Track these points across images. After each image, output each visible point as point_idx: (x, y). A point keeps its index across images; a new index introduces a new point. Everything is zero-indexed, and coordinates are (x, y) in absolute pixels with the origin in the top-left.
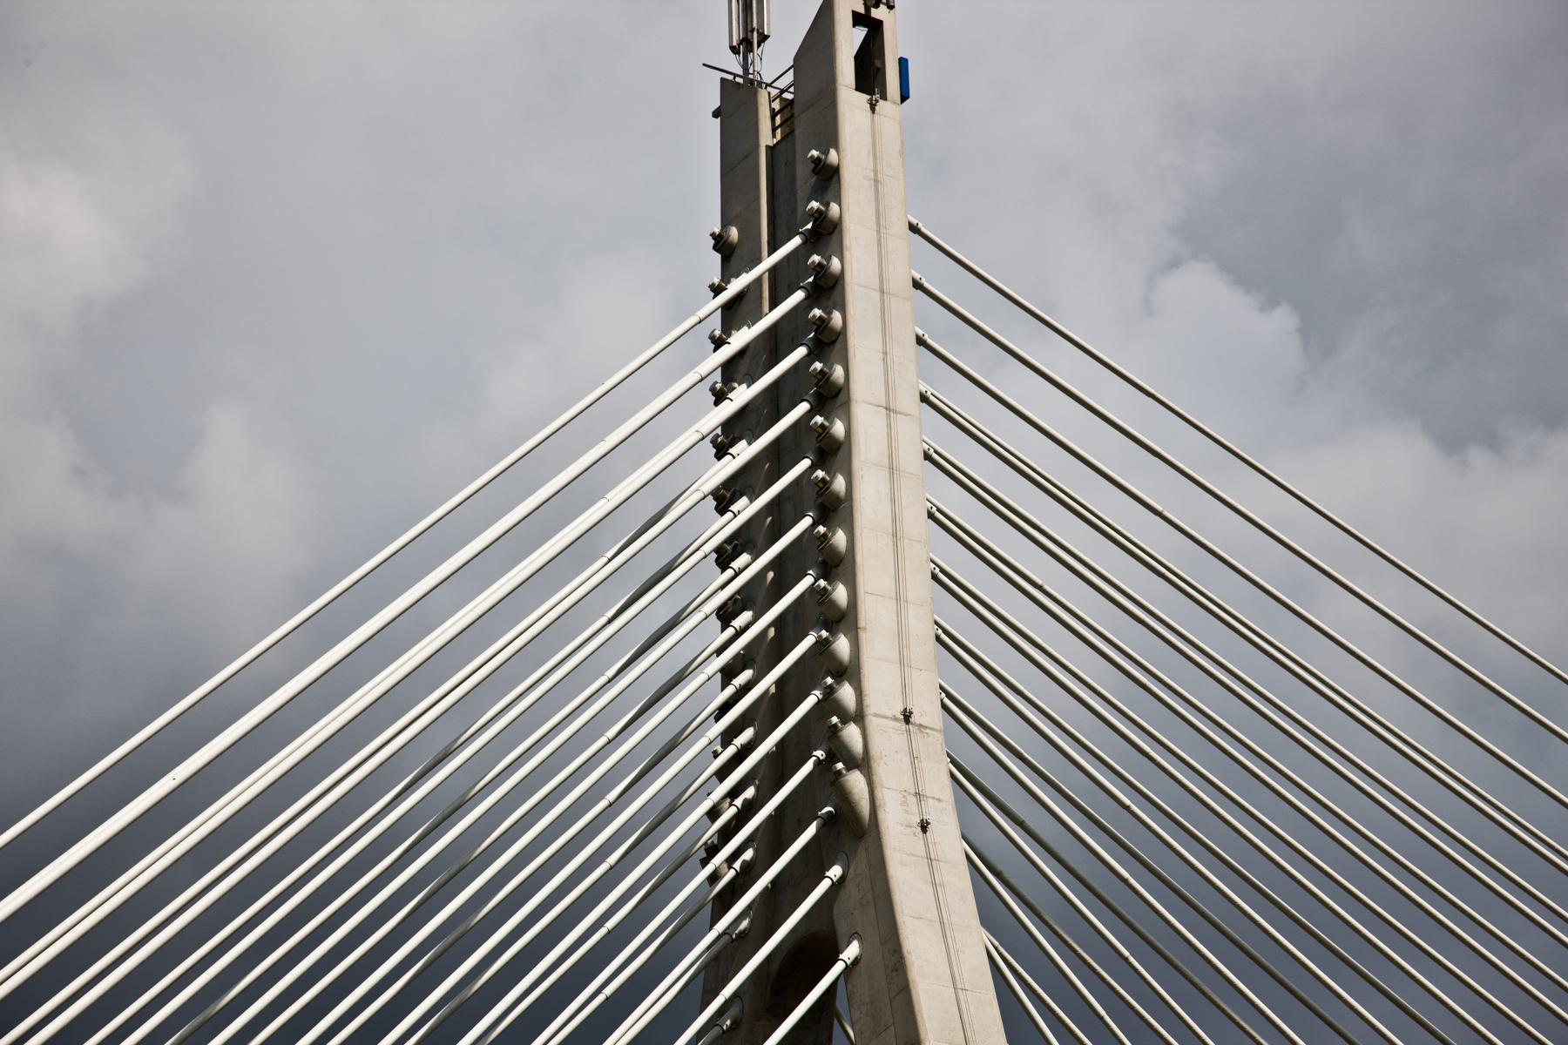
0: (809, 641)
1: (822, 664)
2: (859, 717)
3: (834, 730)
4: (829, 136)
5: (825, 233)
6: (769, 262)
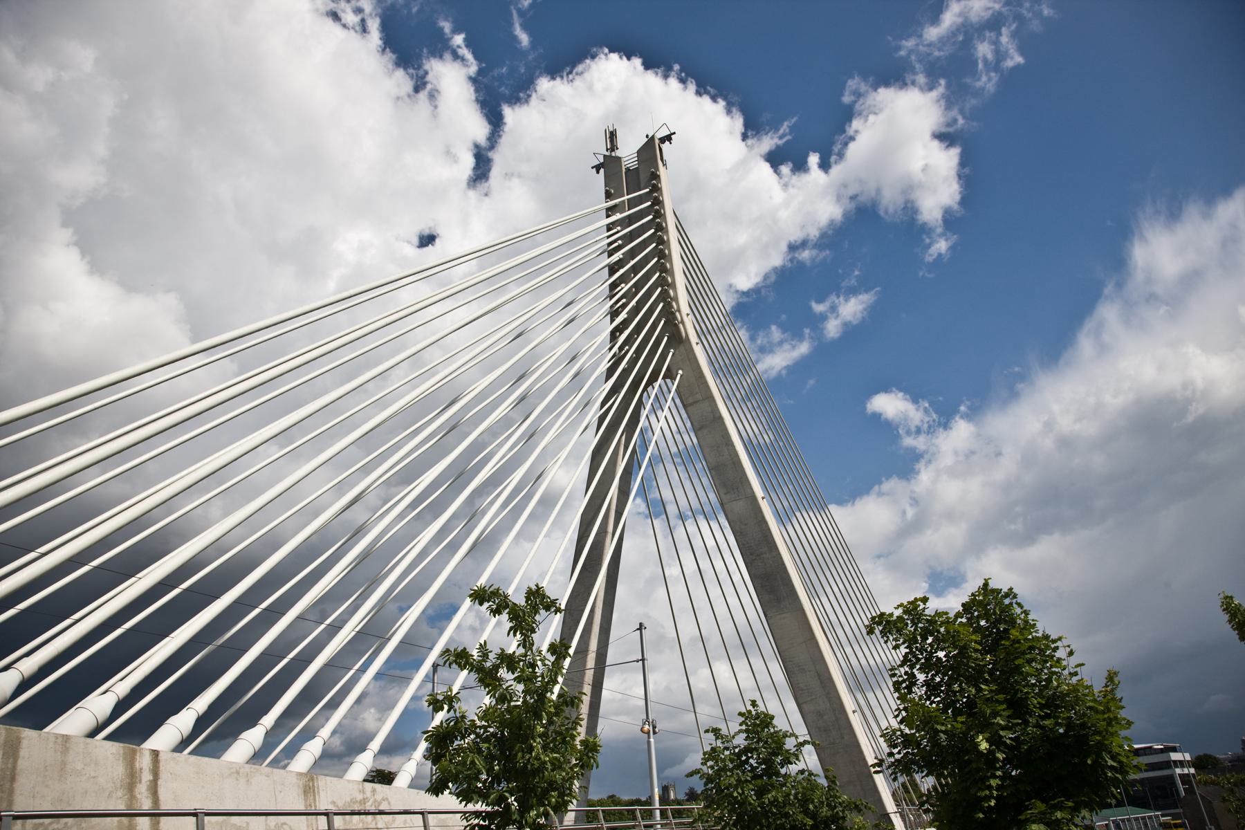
0: (659, 289)
1: (662, 282)
2: (679, 310)
3: (673, 314)
4: (657, 169)
5: (656, 189)
6: (626, 197)
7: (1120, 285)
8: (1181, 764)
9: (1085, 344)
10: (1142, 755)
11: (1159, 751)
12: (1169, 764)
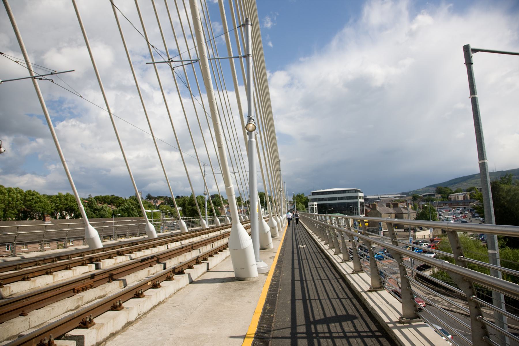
7: (355, 21)
8: (360, 197)
9: (334, 43)
10: (347, 193)
11: (354, 191)
12: (356, 197)
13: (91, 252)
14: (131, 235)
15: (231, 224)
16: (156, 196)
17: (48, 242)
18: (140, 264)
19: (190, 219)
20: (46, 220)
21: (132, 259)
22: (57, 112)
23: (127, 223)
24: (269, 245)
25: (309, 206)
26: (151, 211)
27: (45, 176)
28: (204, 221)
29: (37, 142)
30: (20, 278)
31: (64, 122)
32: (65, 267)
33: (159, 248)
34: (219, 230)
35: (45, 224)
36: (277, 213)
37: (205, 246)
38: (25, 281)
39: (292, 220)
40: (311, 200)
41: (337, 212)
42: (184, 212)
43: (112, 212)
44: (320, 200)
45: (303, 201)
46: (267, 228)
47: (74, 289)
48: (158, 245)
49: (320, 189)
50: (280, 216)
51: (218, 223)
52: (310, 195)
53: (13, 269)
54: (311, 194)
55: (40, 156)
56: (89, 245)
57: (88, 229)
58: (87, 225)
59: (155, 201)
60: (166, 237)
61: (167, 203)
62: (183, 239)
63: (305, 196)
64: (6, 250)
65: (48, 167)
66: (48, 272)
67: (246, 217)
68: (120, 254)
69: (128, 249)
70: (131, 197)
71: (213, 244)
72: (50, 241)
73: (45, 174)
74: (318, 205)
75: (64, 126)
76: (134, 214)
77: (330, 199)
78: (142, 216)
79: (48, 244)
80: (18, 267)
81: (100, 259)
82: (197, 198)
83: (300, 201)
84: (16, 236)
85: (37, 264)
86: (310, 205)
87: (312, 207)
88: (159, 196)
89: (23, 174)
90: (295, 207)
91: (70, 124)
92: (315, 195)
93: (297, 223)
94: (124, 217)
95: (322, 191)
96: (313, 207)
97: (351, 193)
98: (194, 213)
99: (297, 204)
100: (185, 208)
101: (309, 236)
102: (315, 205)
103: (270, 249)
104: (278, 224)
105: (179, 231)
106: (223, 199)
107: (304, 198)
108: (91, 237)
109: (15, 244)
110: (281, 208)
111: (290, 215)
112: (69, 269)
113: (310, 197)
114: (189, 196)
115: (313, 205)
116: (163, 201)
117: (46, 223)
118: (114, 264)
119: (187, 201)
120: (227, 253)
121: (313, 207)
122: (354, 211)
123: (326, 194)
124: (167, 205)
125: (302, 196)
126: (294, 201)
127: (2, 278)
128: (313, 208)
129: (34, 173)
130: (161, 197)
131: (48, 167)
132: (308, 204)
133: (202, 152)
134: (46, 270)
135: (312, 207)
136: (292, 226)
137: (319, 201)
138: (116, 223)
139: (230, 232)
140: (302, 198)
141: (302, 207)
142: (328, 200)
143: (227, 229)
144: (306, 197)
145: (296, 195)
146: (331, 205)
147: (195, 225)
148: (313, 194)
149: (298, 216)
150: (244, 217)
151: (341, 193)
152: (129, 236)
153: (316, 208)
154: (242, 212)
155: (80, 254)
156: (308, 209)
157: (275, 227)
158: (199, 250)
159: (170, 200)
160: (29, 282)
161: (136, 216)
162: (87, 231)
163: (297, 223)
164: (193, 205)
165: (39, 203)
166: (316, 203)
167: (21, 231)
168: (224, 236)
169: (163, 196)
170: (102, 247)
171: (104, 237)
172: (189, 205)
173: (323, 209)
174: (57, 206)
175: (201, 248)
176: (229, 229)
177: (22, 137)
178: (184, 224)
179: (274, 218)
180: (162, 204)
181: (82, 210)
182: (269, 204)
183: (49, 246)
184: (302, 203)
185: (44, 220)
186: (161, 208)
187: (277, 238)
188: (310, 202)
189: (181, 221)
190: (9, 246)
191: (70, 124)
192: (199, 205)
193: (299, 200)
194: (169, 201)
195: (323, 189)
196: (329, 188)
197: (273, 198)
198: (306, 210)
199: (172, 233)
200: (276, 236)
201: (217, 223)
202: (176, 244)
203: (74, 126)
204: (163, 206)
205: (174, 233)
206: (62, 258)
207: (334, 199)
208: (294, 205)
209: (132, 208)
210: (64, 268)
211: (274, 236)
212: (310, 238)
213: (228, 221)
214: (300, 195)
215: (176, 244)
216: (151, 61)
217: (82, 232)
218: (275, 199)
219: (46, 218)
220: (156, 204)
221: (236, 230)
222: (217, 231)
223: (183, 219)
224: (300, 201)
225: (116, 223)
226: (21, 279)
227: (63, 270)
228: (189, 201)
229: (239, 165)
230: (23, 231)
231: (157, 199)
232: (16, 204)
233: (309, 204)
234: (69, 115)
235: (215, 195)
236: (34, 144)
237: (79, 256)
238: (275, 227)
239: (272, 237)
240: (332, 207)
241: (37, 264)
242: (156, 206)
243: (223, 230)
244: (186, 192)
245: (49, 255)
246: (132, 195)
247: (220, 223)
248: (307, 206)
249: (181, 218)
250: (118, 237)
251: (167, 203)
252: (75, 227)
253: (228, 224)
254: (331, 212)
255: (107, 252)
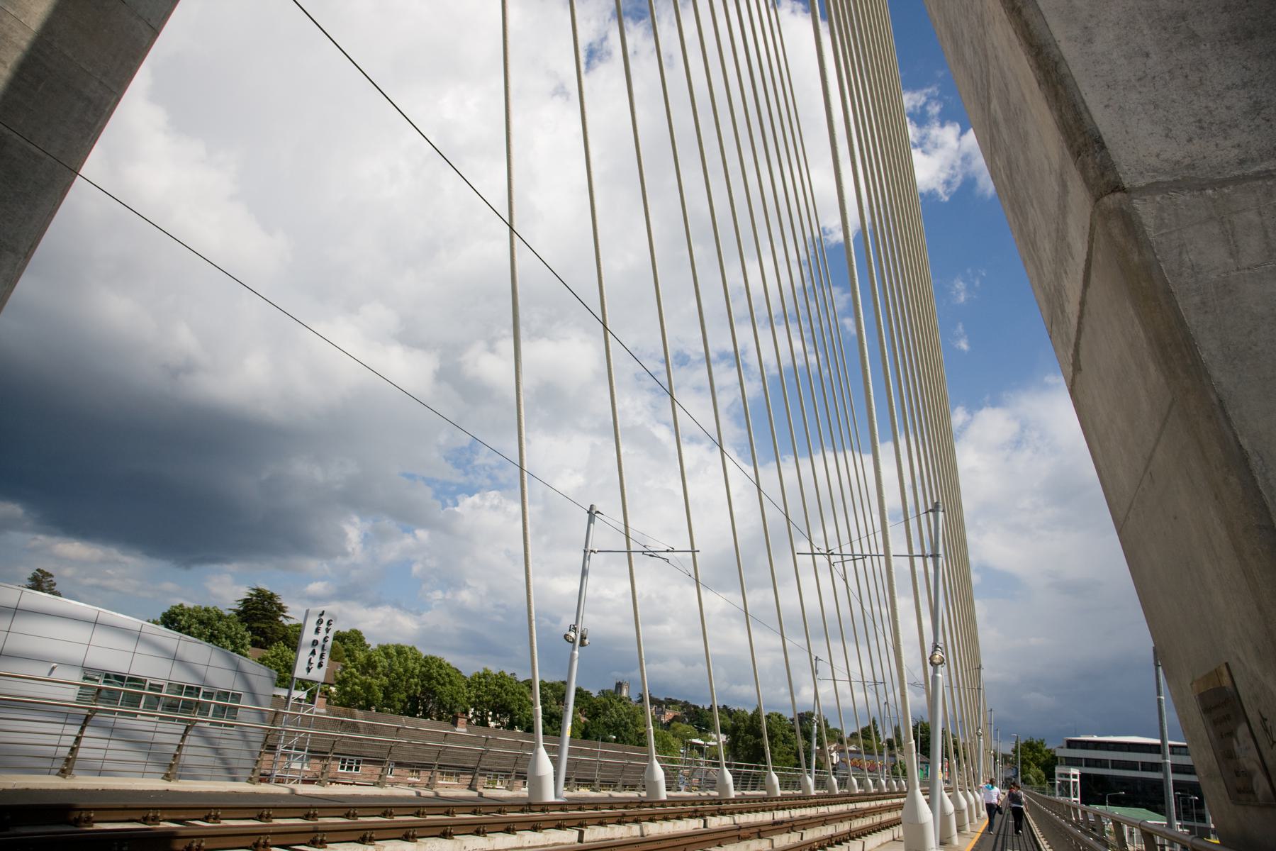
13: (343, 812)
14: (607, 784)
15: (906, 792)
16: (662, 699)
17: (417, 767)
18: (772, 828)
19: (751, 767)
20: (459, 724)
21: (735, 824)
22: (466, 474)
23: (502, 740)
24: (950, 837)
25: (1057, 777)
26: (703, 743)
27: (419, 613)
28: (809, 778)
29: (415, 536)
30: (357, 836)
31: (476, 498)
32: (441, 830)
33: (521, 835)
34: (815, 806)
35: (455, 731)
36: (969, 785)
37: (788, 835)
38: (446, 838)
39: (1001, 813)
40: (1064, 760)
41: (1140, 803)
42: (732, 748)
43: (584, 726)
44: (1090, 763)
45: (1042, 759)
46: (950, 808)
47: (739, 836)
48: (647, 818)
49: (1092, 735)
50: (976, 792)
51: (834, 787)
52: (1062, 748)
53: (301, 815)
54: (1065, 745)
55: (416, 569)
56: (530, 792)
57: (652, 765)
58: (652, 760)
59: (660, 709)
60: (677, 803)
61: (687, 720)
62: (752, 810)
63: (1048, 747)
64: (339, 771)
65: (429, 594)
66: (510, 828)
67: (881, 783)
68: (620, 821)
69: (577, 816)
70: (603, 691)
71: (873, 817)
72: (422, 767)
73: (416, 607)
74: (1083, 776)
75: (474, 507)
76: (628, 739)
77: (1117, 765)
78: (644, 746)
79: (416, 771)
80: (266, 813)
81: (374, 835)
82: (768, 717)
83: (1032, 760)
84: (335, 741)
85: (449, 811)
86: (1061, 775)
87: (1064, 779)
88: (669, 697)
89: (374, 604)
90: (1017, 773)
91: (487, 504)
92: (1075, 748)
93: (1018, 827)
94: (608, 742)
95: (1095, 738)
96: (1067, 779)
97: (1180, 754)
98: (757, 755)
99: (1025, 767)
100: (737, 741)
101: (1032, 839)
102: (1075, 776)
103: (953, 846)
104: (969, 806)
105: (764, 793)
106: (827, 726)
107: (1044, 752)
108: (655, 780)
109: (330, 759)
110: (979, 772)
111: (997, 794)
112: (411, 839)
113: (1059, 753)
114: (750, 712)
115: (1068, 776)
116: (678, 713)
117: (458, 729)
118: (719, 825)
119: (744, 721)
120: (898, 831)
121: (1067, 779)
122: (1192, 808)
123: (1108, 749)
124: (688, 724)
125: (1040, 746)
126: (1016, 757)
127: (271, 831)
128: (1069, 782)
129: (397, 605)
130: (674, 702)
131: (429, 594)
132: (1054, 769)
133: (789, 600)
134: (477, 827)
135: (1064, 779)
136: (998, 835)
137: (1087, 765)
138: (604, 755)
139: (903, 804)
140: (1040, 751)
141: (1038, 778)
142: (1113, 768)
143: (859, 804)
144: (1049, 751)
145: (1023, 742)
146: (1123, 782)
147: (759, 785)
148: (1071, 744)
149: (1024, 799)
150: (887, 781)
151: (1129, 751)
152: (601, 786)
153: (1074, 783)
154: (883, 769)
155: (417, 810)
156: (1054, 785)
157: (963, 811)
158: (836, 827)
159: (696, 712)
160: (415, 844)
161: (631, 743)
162: (532, 760)
163: (1018, 827)
164: (755, 732)
165: (449, 687)
166: (1075, 771)
167: (450, 742)
168: (890, 809)
169: (679, 699)
170: (665, 798)
171: (784, 785)
172: (747, 732)
173: (1095, 790)
174: (478, 697)
175: (837, 824)
176: (841, 806)
177: (387, 523)
178: (729, 778)
179: (949, 797)
180: (675, 718)
181: (537, 717)
182: (953, 765)
183: (418, 778)
184: (1038, 765)
185: (455, 724)
186: (674, 729)
187: (966, 834)
188: (1062, 764)
189: (770, 772)
190: (345, 763)
191: (487, 504)
192: (770, 738)
193: (1030, 757)
194: (698, 719)
195: (1098, 736)
196: (1115, 735)
197: (961, 741)
198: (1046, 786)
199: (743, 794)
200: (964, 830)
201: (831, 788)
202: (721, 819)
203: (495, 508)
204: (678, 726)
205: (747, 795)
206: (532, 808)
207: (1132, 766)
208: (1017, 769)
209: (626, 723)
210: (438, 833)
211: (945, 841)
212: (1032, 842)
213: (870, 787)
214: (1035, 742)
215: (721, 819)
216: (839, 552)
217: (590, 765)
218: (964, 743)
219: (460, 720)
220: (660, 718)
221: (914, 801)
222: (810, 807)
223: (728, 766)
224: (1032, 760)
225: (604, 755)
226: (357, 838)
227: (553, 828)
228: (748, 722)
229: (873, 643)
230: (456, 742)
231: (664, 706)
232: (407, 681)
233: (1058, 770)
234: (488, 482)
235: (806, 713)
236: (408, 541)
237: (342, 814)
238: (963, 811)
239: (977, 817)
240: (1125, 788)
241: (449, 811)
242: (662, 722)
243: (823, 805)
244: (743, 697)
245: (582, 798)
246: (606, 688)
247: (859, 788)
248: (1050, 776)
249: (724, 762)
250: (578, 785)
251: (687, 720)
252: (614, 758)
253: (853, 792)
254: (1123, 802)
255: (603, 811)
